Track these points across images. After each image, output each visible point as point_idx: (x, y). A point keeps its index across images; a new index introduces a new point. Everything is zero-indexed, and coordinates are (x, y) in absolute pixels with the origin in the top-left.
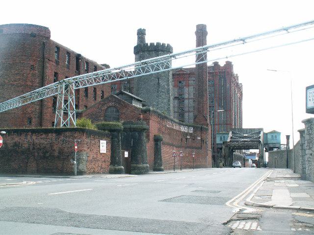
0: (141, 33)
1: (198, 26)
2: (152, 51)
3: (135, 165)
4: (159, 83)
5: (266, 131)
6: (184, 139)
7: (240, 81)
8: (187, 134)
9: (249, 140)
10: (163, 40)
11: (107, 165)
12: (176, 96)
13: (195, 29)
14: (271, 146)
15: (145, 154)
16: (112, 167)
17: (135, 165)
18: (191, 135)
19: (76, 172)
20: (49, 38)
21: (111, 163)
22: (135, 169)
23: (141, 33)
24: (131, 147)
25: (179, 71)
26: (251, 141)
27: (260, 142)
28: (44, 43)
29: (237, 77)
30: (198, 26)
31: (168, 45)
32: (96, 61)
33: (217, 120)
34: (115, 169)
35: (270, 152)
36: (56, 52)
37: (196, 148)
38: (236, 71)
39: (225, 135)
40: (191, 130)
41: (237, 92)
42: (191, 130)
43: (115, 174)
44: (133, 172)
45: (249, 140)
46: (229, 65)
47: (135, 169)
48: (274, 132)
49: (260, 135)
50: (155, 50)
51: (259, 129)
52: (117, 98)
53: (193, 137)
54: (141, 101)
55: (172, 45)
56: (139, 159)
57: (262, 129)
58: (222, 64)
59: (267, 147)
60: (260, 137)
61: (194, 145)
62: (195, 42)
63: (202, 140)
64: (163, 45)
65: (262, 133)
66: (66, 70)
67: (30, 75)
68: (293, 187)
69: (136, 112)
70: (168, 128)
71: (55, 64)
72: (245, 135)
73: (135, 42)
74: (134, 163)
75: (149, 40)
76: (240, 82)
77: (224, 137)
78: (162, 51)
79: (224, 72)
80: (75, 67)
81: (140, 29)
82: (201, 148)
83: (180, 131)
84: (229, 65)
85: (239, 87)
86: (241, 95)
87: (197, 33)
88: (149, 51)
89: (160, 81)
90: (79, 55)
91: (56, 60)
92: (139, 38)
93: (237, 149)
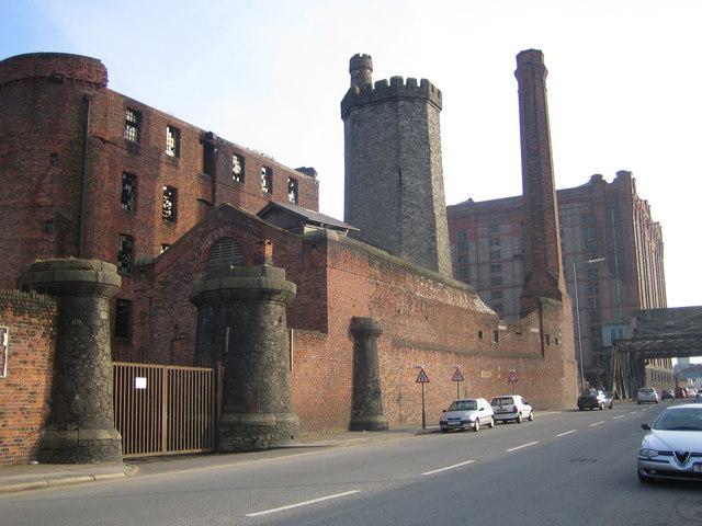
0: (359, 65)
2: (380, 102)
3: (233, 418)
4: (400, 183)
6: (488, 334)
7: (656, 216)
9: (677, 333)
10: (410, 70)
12: (517, 252)
15: (274, 377)
17: (233, 418)
20: (101, 85)
23: (359, 65)
26: (686, 337)
29: (648, 208)
31: (425, 82)
33: (606, 297)
36: (131, 124)
38: (642, 191)
44: (225, 444)
46: (625, 178)
47: (233, 429)
50: (389, 99)
58: (609, 178)
63: (545, 337)
64: (411, 81)
68: (434, 239)
69: (288, 248)
72: (668, 323)
73: (343, 84)
74: (232, 412)
75: (379, 73)
76: (654, 218)
78: (407, 98)
80: (199, 164)
84: (625, 178)
85: (655, 230)
86: (660, 245)
88: (375, 103)
89: (405, 178)
90: (210, 135)
93: (653, 357)
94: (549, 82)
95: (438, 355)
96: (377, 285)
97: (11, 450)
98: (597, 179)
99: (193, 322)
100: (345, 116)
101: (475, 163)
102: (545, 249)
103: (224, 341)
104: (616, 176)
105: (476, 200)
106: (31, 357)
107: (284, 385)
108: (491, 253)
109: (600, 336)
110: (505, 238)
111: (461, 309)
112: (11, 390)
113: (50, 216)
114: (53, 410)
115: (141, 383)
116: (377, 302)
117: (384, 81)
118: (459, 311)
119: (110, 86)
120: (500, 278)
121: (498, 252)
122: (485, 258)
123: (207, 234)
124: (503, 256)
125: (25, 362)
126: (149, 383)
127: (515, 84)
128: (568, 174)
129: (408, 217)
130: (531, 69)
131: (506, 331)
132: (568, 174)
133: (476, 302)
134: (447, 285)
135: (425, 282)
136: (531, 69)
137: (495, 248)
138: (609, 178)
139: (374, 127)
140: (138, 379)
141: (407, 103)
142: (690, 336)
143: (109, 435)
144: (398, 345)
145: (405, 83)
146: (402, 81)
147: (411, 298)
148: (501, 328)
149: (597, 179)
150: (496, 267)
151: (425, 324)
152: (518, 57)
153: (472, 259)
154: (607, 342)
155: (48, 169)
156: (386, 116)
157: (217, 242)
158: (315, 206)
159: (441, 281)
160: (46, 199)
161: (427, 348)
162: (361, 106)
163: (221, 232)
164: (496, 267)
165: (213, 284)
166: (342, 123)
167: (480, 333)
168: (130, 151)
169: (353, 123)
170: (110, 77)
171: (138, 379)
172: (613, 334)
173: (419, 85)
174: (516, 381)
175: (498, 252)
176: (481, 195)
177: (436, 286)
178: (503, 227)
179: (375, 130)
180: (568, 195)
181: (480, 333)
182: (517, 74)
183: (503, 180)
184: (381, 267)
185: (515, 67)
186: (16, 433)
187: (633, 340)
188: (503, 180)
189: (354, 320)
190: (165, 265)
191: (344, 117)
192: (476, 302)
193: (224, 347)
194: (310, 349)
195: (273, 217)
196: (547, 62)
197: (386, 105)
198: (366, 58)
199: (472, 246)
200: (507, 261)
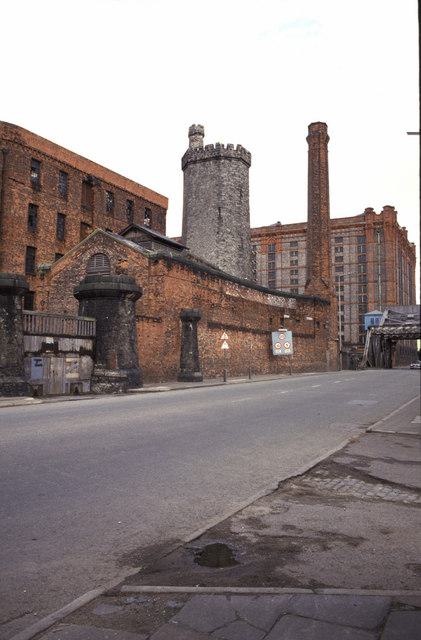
0: (195, 133)
4: (220, 218)
8: (282, 311)
18: (292, 312)
23: (195, 133)
46: (390, 211)
57: (194, 126)
58: (378, 210)
63: (317, 322)
70: (229, 298)
73: (183, 145)
75: (209, 140)
78: (226, 158)
79: (382, 223)
98: (369, 211)
99: (76, 308)
101: (276, 198)
118: (255, 304)
121: (297, 261)
122: (287, 265)
127: (305, 147)
128: (344, 205)
130: (318, 136)
132: (344, 205)
136: (318, 136)
137: (295, 258)
138: (378, 210)
143: (70, 368)
148: (285, 316)
149: (369, 211)
153: (278, 265)
156: (214, 167)
158: (164, 233)
162: (175, 608)
163: (96, 250)
164: (294, 272)
165: (90, 286)
166: (182, 173)
168: (34, 188)
180: (346, 224)
182: (309, 139)
183: (296, 212)
185: (307, 135)
188: (296, 212)
195: (132, 235)
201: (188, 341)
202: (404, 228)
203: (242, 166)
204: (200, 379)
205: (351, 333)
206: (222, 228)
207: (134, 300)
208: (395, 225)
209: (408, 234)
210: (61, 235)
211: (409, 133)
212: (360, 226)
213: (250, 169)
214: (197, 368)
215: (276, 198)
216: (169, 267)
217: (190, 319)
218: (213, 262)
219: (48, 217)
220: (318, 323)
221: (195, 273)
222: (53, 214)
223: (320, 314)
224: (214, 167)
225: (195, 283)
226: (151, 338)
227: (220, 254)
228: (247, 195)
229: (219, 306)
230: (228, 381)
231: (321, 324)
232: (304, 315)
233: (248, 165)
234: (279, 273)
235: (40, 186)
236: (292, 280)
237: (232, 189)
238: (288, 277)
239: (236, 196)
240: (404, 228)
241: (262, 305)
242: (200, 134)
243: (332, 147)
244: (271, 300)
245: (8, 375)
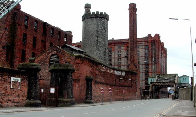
0: (88, 7)
1: (130, 5)
4: (97, 40)
5: (179, 75)
6: (118, 80)
8: (120, 76)
9: (168, 81)
11: (24, 99)
12: (126, 55)
13: (128, 7)
14: (183, 85)
16: (28, 101)
18: (123, 77)
19: (148, 90)
20: (20, 10)
21: (28, 98)
22: (60, 103)
23: (88, 7)
24: (59, 85)
25: (127, 41)
26: (169, 82)
27: (174, 82)
28: (109, 44)
30: (130, 5)
31: (105, 13)
32: (60, 28)
34: (31, 103)
35: (179, 89)
37: (127, 86)
38: (162, 40)
39: (153, 78)
40: (124, 74)
41: (163, 53)
42: (124, 74)
43: (30, 107)
44: (59, 105)
45: (168, 81)
46: (157, 36)
47: (61, 102)
48: (185, 76)
49: (175, 78)
50: (95, 17)
51: (175, 74)
52: (58, 48)
53: (125, 78)
54: (83, 52)
55: (108, 14)
56: (64, 94)
57: (177, 74)
58: (153, 35)
59: (180, 86)
60: (175, 79)
61: (126, 84)
62: (129, 15)
63: (132, 81)
64: (101, 13)
65: (176, 77)
66: (34, 32)
67: (4, 35)
70: (102, 72)
71: (24, 28)
72: (166, 78)
73: (83, 12)
74: (61, 98)
75: (93, 10)
77: (153, 79)
78: (100, 17)
79: (155, 41)
81: (87, 4)
82: (131, 86)
83: (115, 74)
84: (157, 36)
87: (129, 9)
91: (25, 25)
92: (86, 10)
94: (137, 12)
95: (105, 85)
96: (92, 68)
97: (21, 104)
98: (150, 35)
100: (83, 20)
101: (117, 31)
102: (134, 58)
103: (59, 81)
104: (155, 35)
105: (115, 39)
106: (24, 85)
107: (72, 92)
108: (118, 55)
109: (148, 81)
110: (123, 51)
111: (112, 74)
112: (21, 91)
113: (5, 45)
114: (28, 96)
115: (42, 91)
116: (91, 72)
117: (95, 12)
119: (21, 10)
120: (120, 63)
122: (116, 56)
123: (49, 53)
124: (122, 64)
125: (23, 86)
126: (41, 90)
128: (141, 34)
129: (99, 49)
130: (133, 9)
131: (123, 80)
132: (141, 34)
133: (115, 72)
134: (108, 67)
135: (103, 66)
136: (133, 9)
137: (120, 54)
138: (153, 35)
139: (91, 24)
140: (51, 92)
141: (100, 19)
142: (171, 82)
144: (96, 83)
145: (100, 13)
146: (99, 13)
147: (99, 71)
149: (150, 35)
150: (119, 59)
151: (102, 78)
152: (129, 5)
153: (113, 56)
154: (149, 83)
155: (5, 32)
156: (95, 20)
157: (52, 55)
159: (107, 66)
160: (4, 40)
161: (102, 83)
163: (53, 53)
164: (119, 59)
166: (82, 22)
167: (116, 80)
169: (85, 22)
170: (21, 7)
171: (51, 92)
172: (151, 80)
173: (103, 14)
174: (120, 92)
175: (120, 55)
176: (116, 38)
177: (105, 68)
178: (123, 47)
179: (91, 25)
181: (116, 80)
184: (93, 63)
186: (22, 101)
187: (156, 82)
189: (86, 76)
190: (38, 60)
191: (83, 20)
192: (115, 72)
193: (58, 83)
194: (76, 84)
195: (65, 48)
196: (137, 7)
197: (94, 19)
198: (90, 5)
199: (113, 53)
200: (123, 58)
201: (89, 88)
202: (163, 42)
203: (106, 21)
204: (92, 103)
205: (142, 85)
206: (98, 44)
207: (72, 73)
208: (159, 42)
209: (164, 45)
210: (34, 45)
211: (170, 19)
212: (146, 41)
213: (109, 22)
214: (92, 99)
215: (117, 31)
216: (82, 60)
217: (88, 80)
218: (95, 57)
219: (30, 39)
220: (133, 81)
221: (91, 62)
222: (32, 37)
223: (134, 78)
224: (95, 20)
225: (91, 66)
226: (77, 89)
227: (95, 54)
228: (107, 32)
229: (98, 75)
230: (103, 104)
231: (134, 82)
232: (128, 78)
233: (108, 20)
234: (113, 60)
235: (28, 26)
236: (118, 63)
237: (102, 29)
238: (116, 61)
239: (104, 32)
240: (163, 42)
241: (113, 74)
242: (105, 18)
243: (138, 13)
244: (117, 73)
245: (35, 100)
